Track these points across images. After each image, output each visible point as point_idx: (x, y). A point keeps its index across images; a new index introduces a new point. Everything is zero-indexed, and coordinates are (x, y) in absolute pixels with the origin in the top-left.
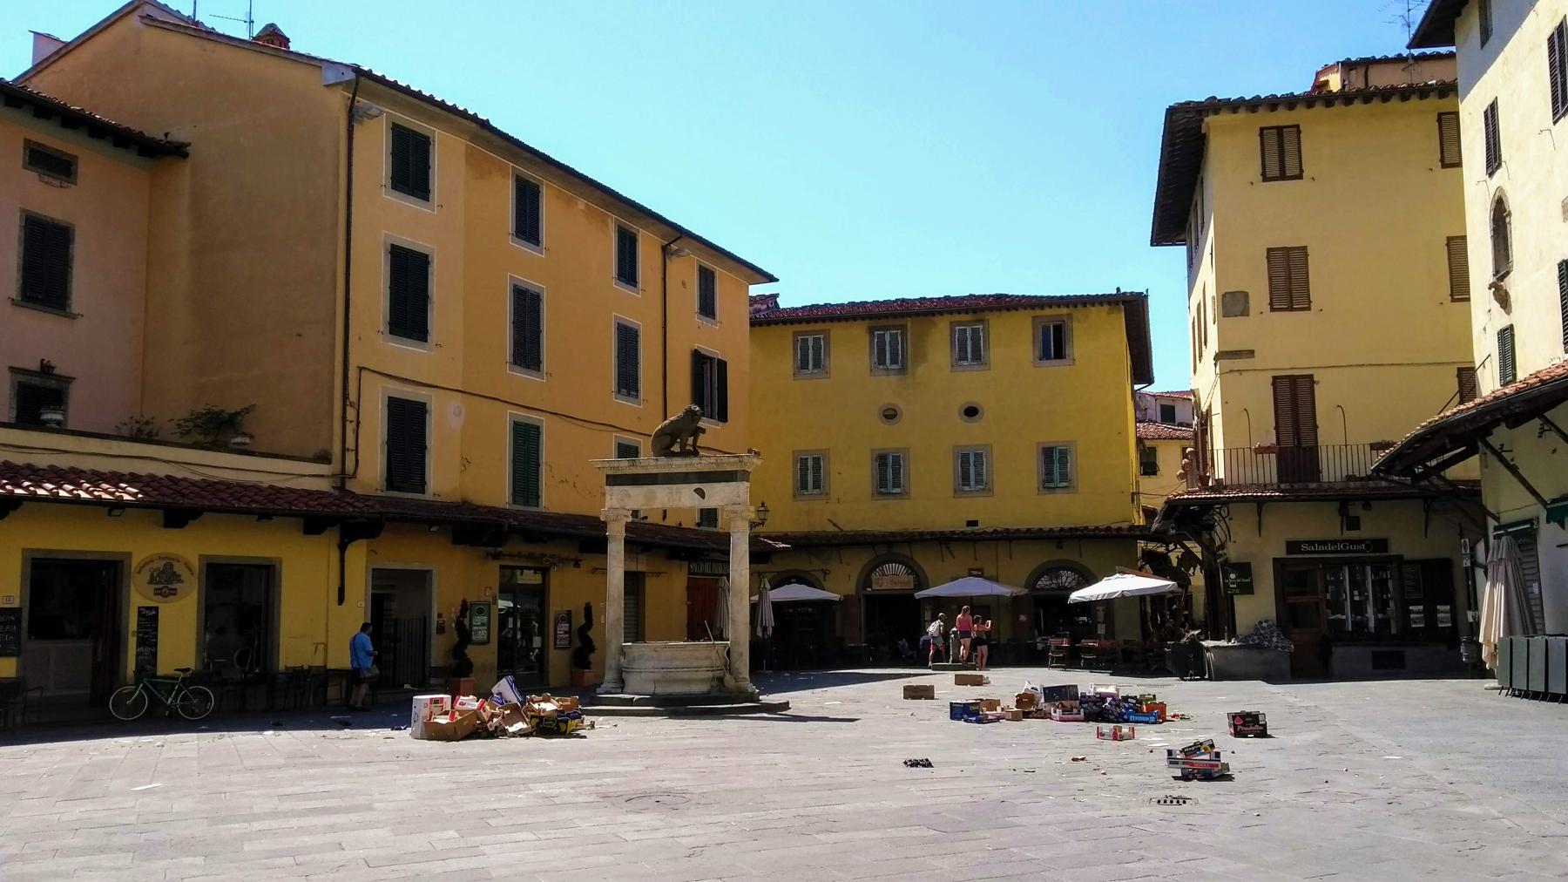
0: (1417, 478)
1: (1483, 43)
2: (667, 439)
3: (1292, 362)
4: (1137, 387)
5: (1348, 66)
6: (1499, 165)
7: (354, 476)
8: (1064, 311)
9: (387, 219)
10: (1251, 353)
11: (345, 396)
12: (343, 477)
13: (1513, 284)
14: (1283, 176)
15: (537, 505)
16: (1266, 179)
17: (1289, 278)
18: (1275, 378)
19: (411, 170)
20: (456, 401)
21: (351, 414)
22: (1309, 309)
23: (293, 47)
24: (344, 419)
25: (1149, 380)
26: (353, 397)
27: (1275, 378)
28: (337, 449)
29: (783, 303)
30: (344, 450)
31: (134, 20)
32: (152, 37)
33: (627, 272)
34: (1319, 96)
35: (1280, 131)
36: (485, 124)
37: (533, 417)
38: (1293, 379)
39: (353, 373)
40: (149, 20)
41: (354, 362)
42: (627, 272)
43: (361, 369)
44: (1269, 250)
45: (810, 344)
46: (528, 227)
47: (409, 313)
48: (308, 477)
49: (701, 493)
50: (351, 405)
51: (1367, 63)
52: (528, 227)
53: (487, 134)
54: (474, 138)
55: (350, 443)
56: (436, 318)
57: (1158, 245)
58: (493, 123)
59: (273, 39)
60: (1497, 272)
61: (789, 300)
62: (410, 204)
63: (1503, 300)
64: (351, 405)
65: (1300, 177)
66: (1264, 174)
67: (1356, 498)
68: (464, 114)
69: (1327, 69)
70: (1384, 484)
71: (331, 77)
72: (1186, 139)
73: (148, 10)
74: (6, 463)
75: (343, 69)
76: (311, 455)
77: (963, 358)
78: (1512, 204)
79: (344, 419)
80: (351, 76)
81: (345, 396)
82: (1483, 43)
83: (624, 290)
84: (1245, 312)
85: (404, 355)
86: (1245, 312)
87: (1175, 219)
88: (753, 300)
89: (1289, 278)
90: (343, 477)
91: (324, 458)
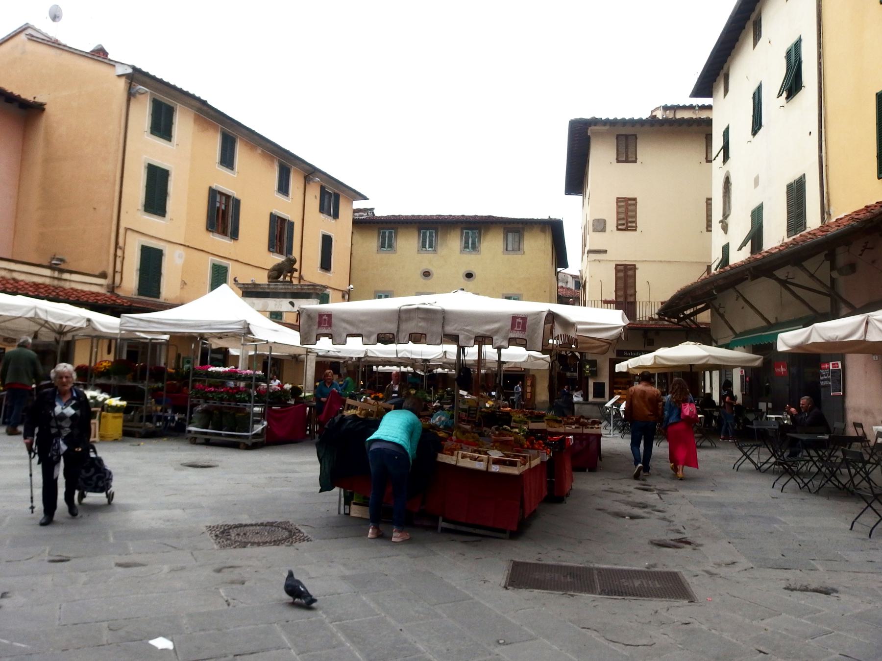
0: (680, 320)
1: (725, 95)
2: (275, 273)
3: (627, 258)
4: (559, 269)
5: (666, 108)
6: (790, 187)
7: (119, 287)
8: (521, 226)
9: (146, 149)
10: (605, 251)
11: (117, 243)
12: (112, 288)
13: (730, 220)
14: (627, 161)
15: (158, 297)
16: (618, 161)
17: (627, 214)
18: (617, 265)
19: (162, 126)
20: (180, 250)
21: (119, 253)
22: (635, 230)
23: (110, 57)
24: (115, 255)
25: (565, 266)
26: (121, 243)
27: (617, 265)
28: (110, 271)
29: (378, 213)
30: (115, 272)
31: (23, 37)
32: (32, 47)
33: (284, 188)
34: (652, 122)
35: (628, 136)
36: (204, 103)
37: (224, 262)
38: (626, 266)
39: (122, 231)
40: (32, 38)
41: (123, 225)
42: (284, 188)
43: (127, 229)
44: (618, 199)
45: (387, 234)
46: (227, 160)
47: (156, 199)
48: (95, 286)
49: (292, 304)
50: (120, 248)
51: (676, 108)
52: (227, 160)
53: (205, 108)
54: (199, 110)
55: (118, 268)
56: (171, 204)
57: (569, 194)
58: (209, 102)
59: (100, 54)
60: (724, 215)
61: (381, 212)
62: (159, 142)
63: (725, 228)
64: (120, 248)
65: (635, 162)
66: (617, 159)
67: (652, 329)
68: (193, 97)
69: (657, 109)
70: (666, 323)
71: (120, 70)
72: (582, 137)
73: (29, 31)
74: (3, 278)
75: (126, 67)
76: (97, 273)
77: (466, 247)
78: (733, 180)
79: (115, 255)
80: (130, 71)
81: (117, 243)
82: (725, 95)
83: (281, 197)
84: (603, 230)
85: (151, 223)
86: (603, 230)
87: (576, 182)
88: (355, 211)
89: (627, 214)
90: (112, 288)
91: (103, 275)
